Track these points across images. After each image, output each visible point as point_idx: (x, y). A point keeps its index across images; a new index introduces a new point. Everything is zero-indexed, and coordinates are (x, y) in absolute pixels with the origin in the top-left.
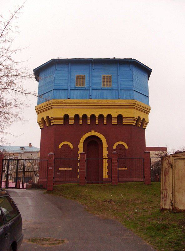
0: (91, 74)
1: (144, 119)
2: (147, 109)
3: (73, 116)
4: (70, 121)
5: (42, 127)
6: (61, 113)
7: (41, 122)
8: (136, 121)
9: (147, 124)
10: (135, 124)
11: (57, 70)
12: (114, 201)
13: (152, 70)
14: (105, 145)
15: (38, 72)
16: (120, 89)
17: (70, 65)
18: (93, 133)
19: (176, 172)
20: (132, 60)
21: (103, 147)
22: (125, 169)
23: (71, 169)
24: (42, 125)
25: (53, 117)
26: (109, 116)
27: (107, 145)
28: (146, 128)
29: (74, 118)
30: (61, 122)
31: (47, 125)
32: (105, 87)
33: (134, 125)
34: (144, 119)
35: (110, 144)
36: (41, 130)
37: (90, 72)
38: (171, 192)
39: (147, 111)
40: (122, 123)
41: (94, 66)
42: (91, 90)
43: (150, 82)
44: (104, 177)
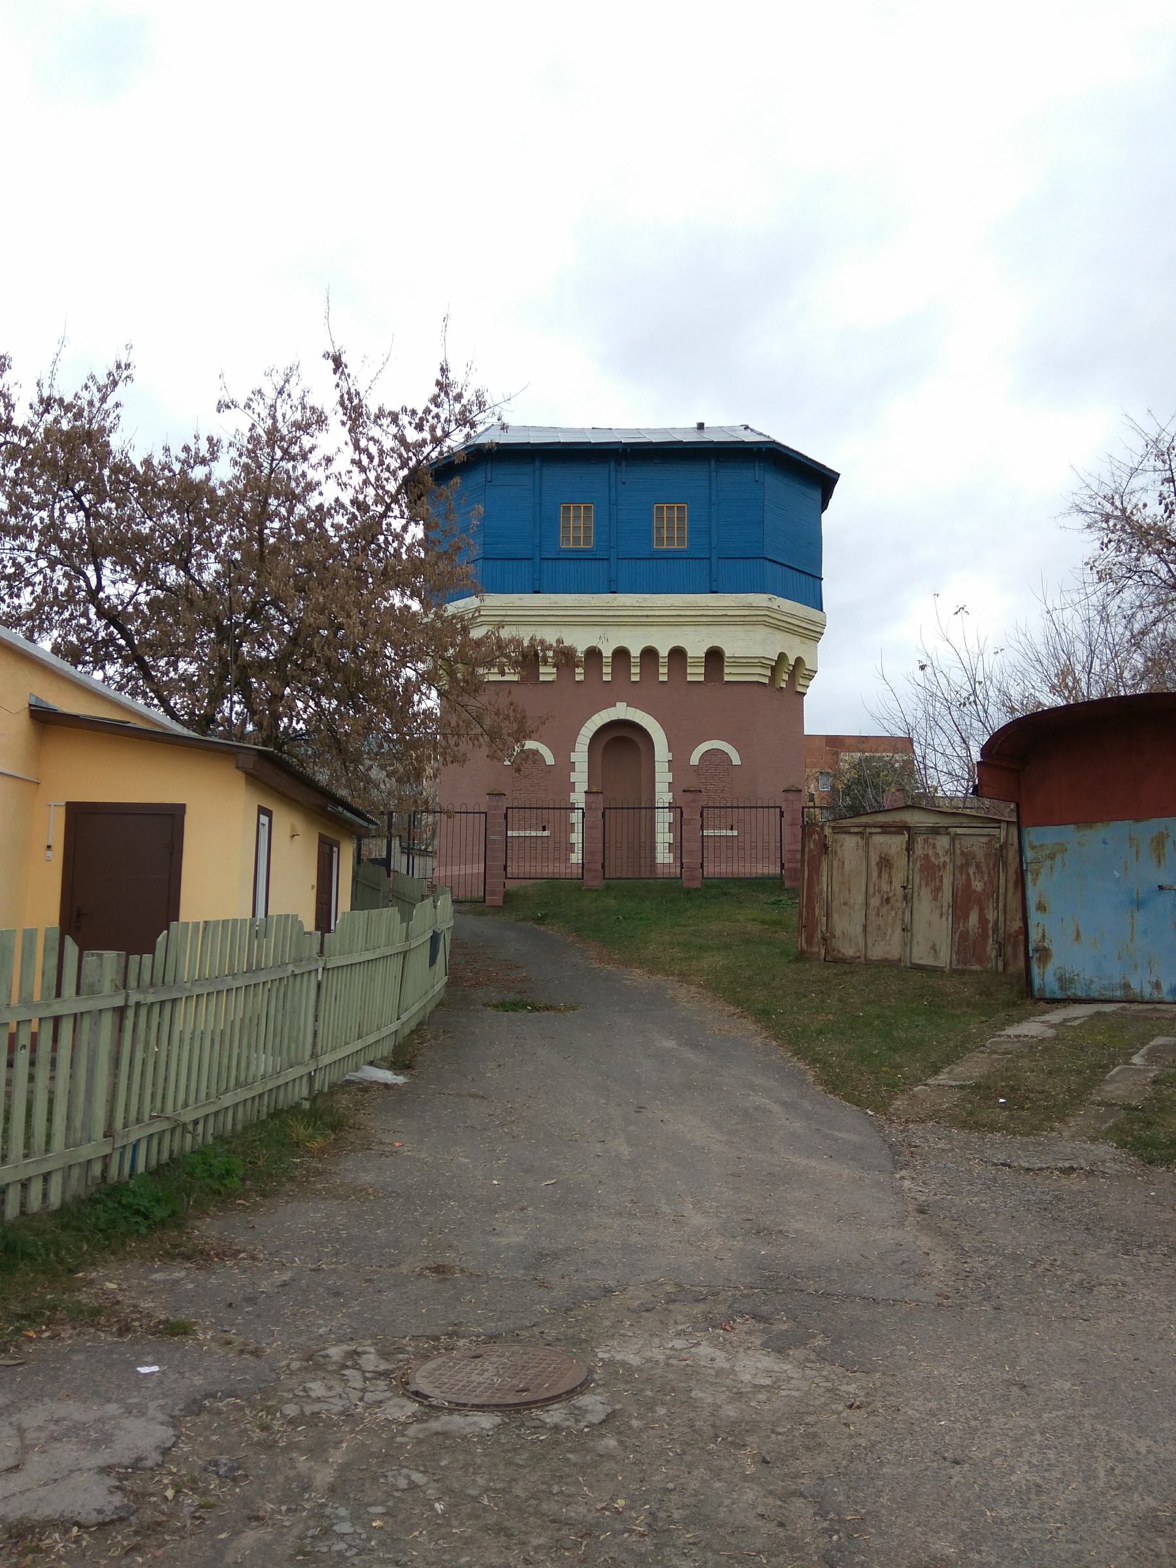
1: (799, 661)
8: (773, 669)
9: (811, 678)
10: (766, 681)
13: (838, 475)
18: (621, 711)
19: (835, 863)
22: (729, 833)
23: (546, 833)
26: (678, 654)
28: (808, 691)
34: (799, 661)
35: (680, 746)
37: (610, 493)
38: (824, 912)
43: (825, 516)
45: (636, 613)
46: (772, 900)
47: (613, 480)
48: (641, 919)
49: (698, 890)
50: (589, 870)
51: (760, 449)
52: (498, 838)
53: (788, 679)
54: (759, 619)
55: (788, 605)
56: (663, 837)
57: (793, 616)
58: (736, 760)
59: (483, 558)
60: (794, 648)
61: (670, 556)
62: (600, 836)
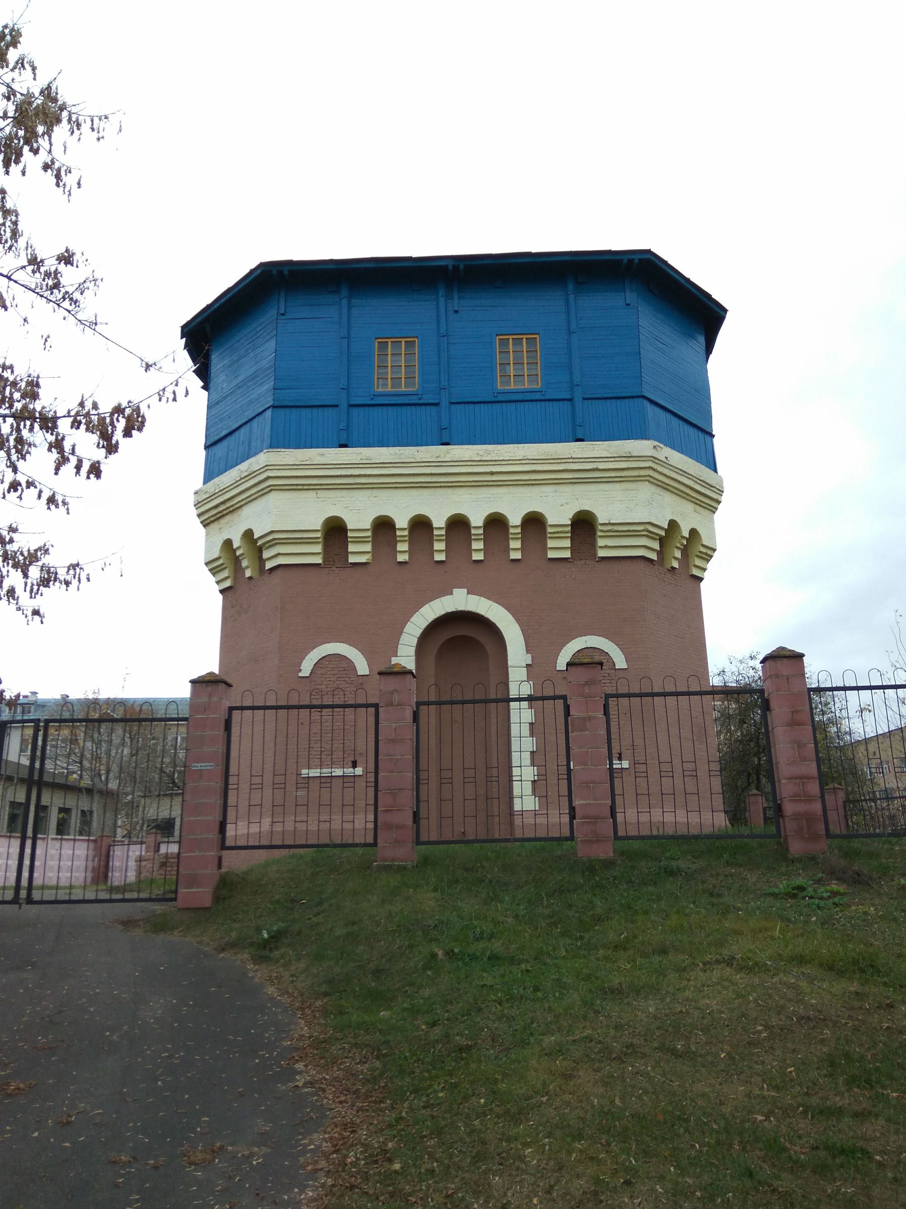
0: (442, 331)
1: (694, 532)
3: (368, 525)
4: (352, 548)
5: (228, 584)
8: (662, 540)
9: (708, 558)
10: (654, 556)
11: (289, 316)
13: (725, 311)
15: (204, 336)
16: (578, 394)
17: (344, 292)
18: (460, 600)
20: (637, 257)
21: (510, 663)
23: (359, 771)
24: (225, 574)
25: (272, 532)
27: (528, 651)
28: (706, 575)
30: (314, 554)
31: (248, 573)
33: (519, 560)
34: (694, 532)
35: (541, 643)
36: (221, 597)
37: (438, 323)
39: (708, 500)
40: (595, 554)
42: (444, 403)
46: (782, 886)
47: (443, 311)
49: (608, 864)
50: (389, 827)
53: (679, 559)
54: (642, 473)
55: (677, 458)
56: (524, 773)
57: (684, 473)
58: (620, 662)
59: (274, 407)
62: (409, 757)
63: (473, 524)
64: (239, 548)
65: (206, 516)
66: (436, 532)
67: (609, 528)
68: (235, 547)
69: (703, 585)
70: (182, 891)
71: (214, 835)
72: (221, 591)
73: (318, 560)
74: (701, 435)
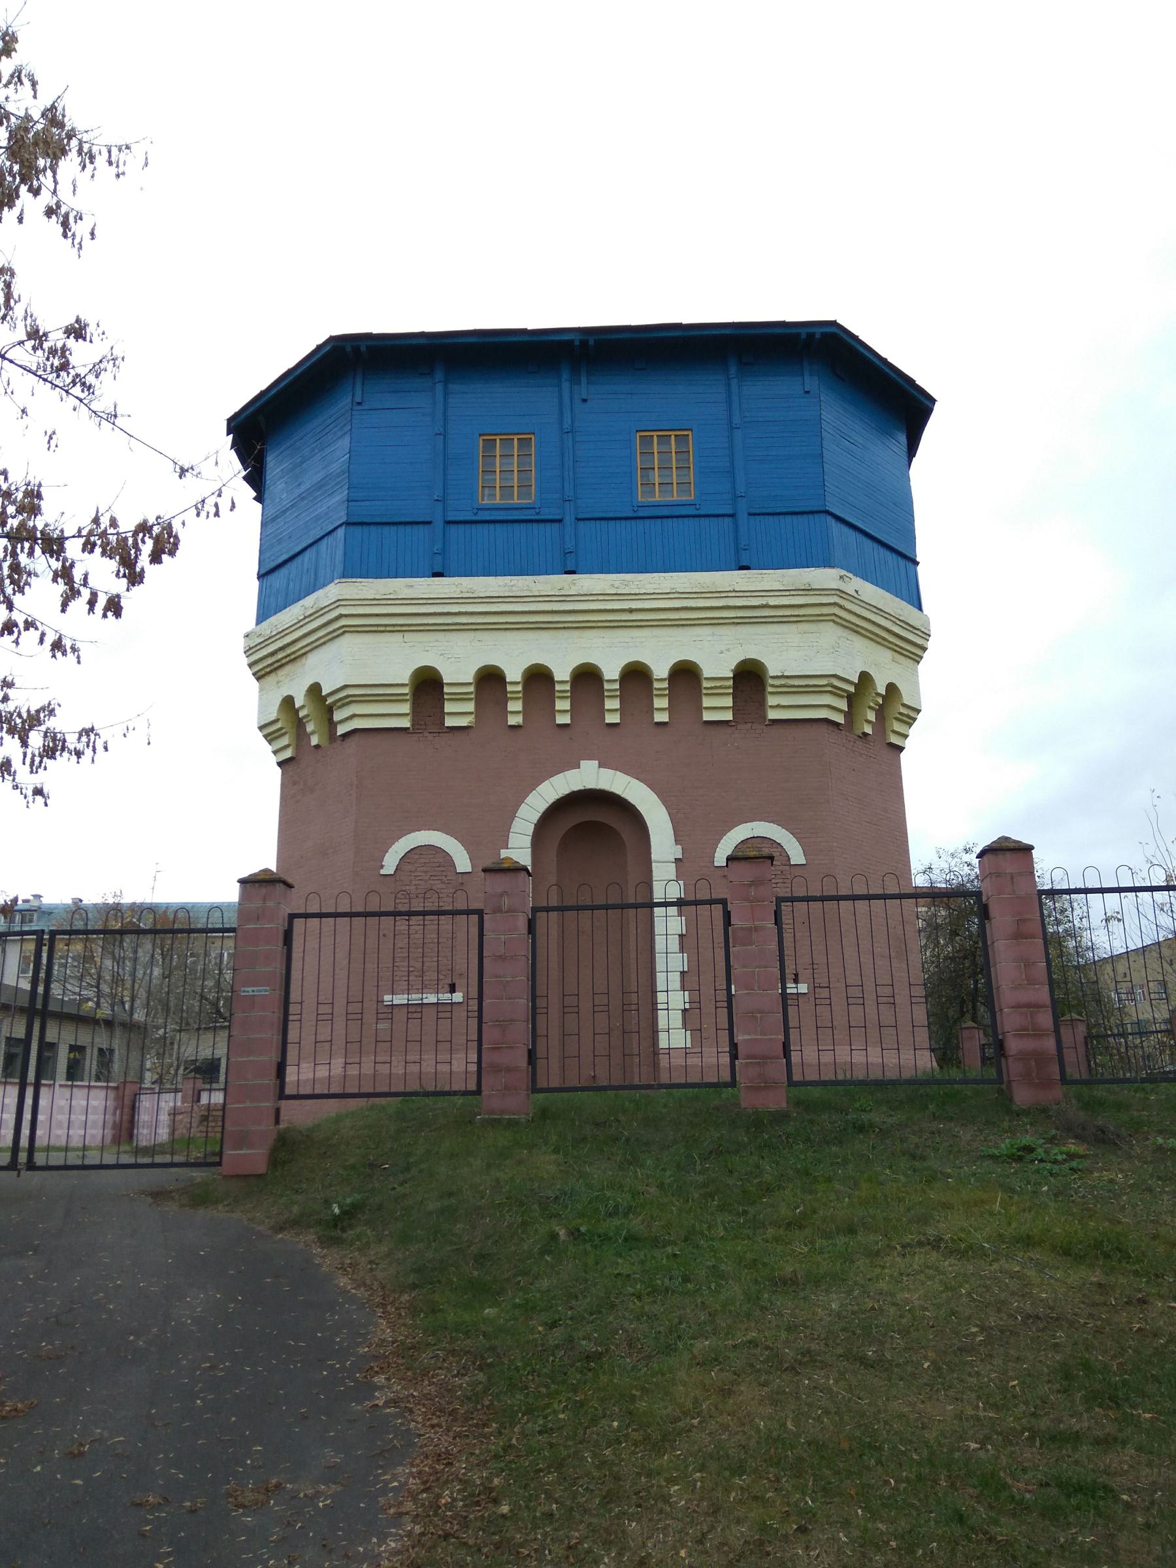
1: (892, 688)
2: (913, 628)
3: (469, 677)
4: (449, 707)
5: (288, 754)
6: (393, 662)
7: (279, 725)
8: (850, 698)
9: (910, 721)
10: (840, 719)
12: (982, 927)
13: (933, 401)
14: (664, 845)
15: (259, 431)
16: (743, 507)
17: (439, 375)
18: (590, 775)
20: (818, 331)
21: (654, 857)
23: (458, 997)
24: (285, 741)
25: (346, 687)
26: (685, 675)
28: (908, 744)
29: (472, 689)
30: (399, 715)
31: (314, 740)
32: (657, 498)
34: (892, 688)
35: (693, 832)
36: (279, 771)
39: (910, 645)
41: (584, 379)
42: (569, 519)
43: (911, 472)
44: (661, 1046)
45: (609, 606)
48: (632, 1239)
49: (780, 1117)
50: (497, 1069)
51: (811, 336)
52: (262, 991)
53: (873, 721)
54: (826, 610)
55: (870, 592)
56: (672, 999)
57: (879, 611)
58: (797, 856)
59: (347, 524)
60: (885, 670)
61: (665, 512)
62: (523, 978)
63: (607, 676)
64: (303, 707)
65: (260, 666)
66: (558, 687)
67: (782, 682)
68: (297, 706)
69: (902, 755)
70: (229, 1152)
71: (270, 1081)
72: (280, 764)
73: (406, 723)
74: (902, 562)
